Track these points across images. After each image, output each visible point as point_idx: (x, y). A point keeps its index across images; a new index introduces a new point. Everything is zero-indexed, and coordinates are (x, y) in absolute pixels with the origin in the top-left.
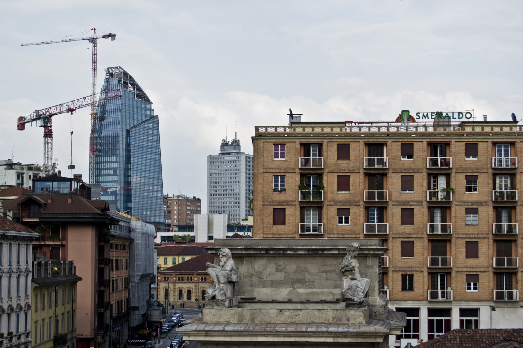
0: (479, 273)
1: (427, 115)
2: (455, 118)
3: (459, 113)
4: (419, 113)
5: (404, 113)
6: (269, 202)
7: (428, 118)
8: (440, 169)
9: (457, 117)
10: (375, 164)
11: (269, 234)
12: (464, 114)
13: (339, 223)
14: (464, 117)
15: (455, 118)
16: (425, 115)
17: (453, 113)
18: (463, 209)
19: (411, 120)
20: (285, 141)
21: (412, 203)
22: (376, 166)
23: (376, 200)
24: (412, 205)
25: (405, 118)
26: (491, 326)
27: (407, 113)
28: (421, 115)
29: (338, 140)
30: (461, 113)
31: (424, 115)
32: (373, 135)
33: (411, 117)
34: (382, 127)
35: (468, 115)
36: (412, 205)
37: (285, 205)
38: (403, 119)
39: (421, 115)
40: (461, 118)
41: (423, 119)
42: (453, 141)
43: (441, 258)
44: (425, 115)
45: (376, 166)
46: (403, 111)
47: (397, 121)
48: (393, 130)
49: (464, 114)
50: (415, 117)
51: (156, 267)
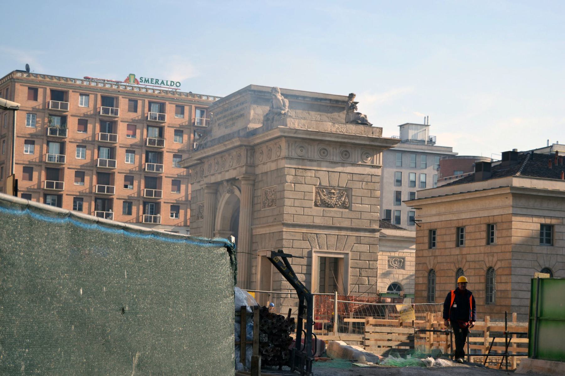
0: (180, 205)
1: (148, 80)
2: (168, 85)
3: (171, 82)
4: (142, 78)
5: (131, 76)
6: (22, 134)
7: (149, 83)
8: (157, 122)
9: (169, 84)
10: (109, 113)
11: (20, 161)
12: (175, 83)
13: (126, 162)
14: (175, 85)
15: (168, 85)
16: (147, 79)
17: (167, 81)
18: (124, 150)
19: (136, 82)
20: (38, 86)
21: (134, 147)
22: (110, 115)
23: (156, 146)
24: (134, 148)
25: (132, 80)
26: (541, 268)
27: (134, 76)
28: (144, 79)
29: (81, 91)
30: (173, 82)
31: (145, 80)
32: (107, 90)
33: (136, 79)
34: (149, 89)
35: (178, 84)
36: (134, 148)
37: (35, 138)
38: (130, 81)
39: (144, 79)
40: (172, 86)
41: (145, 82)
42: (167, 103)
43: (56, 182)
44: (147, 79)
45: (110, 115)
46: (130, 74)
47: (125, 81)
48: (121, 88)
49: (175, 83)
50: (139, 80)
51: (464, 224)
